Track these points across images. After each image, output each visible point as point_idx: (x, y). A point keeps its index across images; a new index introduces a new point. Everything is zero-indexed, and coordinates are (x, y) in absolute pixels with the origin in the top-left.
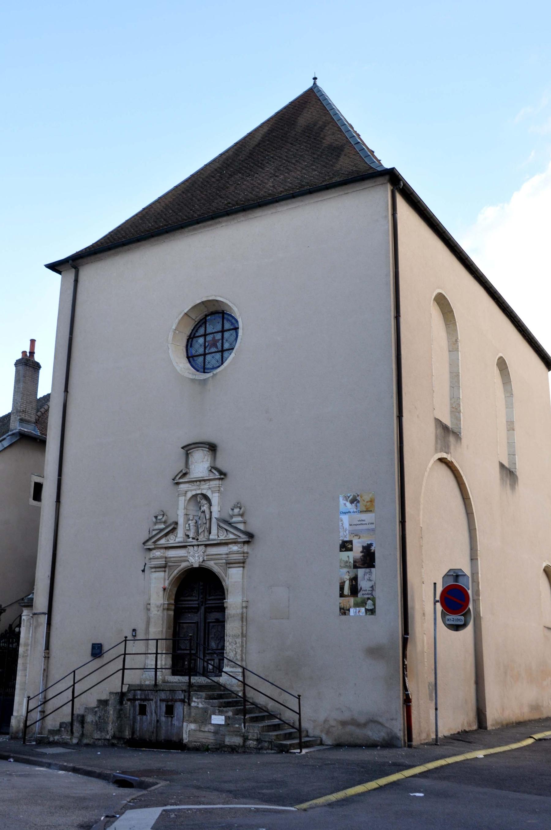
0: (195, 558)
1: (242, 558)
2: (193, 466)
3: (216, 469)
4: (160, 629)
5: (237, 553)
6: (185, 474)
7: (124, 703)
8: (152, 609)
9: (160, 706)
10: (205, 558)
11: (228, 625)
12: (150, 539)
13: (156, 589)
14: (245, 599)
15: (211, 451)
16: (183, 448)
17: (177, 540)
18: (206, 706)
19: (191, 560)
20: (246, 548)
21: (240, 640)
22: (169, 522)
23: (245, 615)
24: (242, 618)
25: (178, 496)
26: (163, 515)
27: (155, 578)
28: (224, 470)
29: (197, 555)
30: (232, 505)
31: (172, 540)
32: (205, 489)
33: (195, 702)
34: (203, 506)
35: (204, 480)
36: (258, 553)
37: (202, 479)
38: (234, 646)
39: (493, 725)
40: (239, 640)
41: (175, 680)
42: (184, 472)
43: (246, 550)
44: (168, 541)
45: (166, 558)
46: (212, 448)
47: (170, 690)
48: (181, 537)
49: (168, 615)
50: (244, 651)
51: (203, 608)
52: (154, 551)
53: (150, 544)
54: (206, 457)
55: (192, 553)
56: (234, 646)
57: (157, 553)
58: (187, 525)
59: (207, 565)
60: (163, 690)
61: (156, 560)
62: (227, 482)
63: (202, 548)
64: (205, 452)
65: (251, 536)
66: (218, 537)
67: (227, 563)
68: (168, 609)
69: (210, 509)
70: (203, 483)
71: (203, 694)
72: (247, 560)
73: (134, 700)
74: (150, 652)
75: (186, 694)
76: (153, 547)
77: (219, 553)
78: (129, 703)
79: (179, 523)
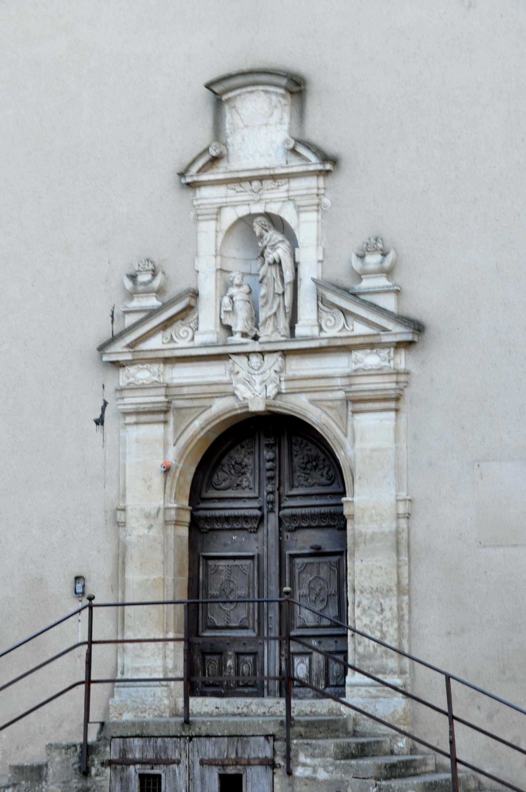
0: (254, 389)
1: (393, 386)
2: (239, 137)
3: (309, 146)
4: (158, 575)
5: (379, 372)
6: (215, 160)
7: (93, 771)
8: (132, 523)
9: (202, 779)
10: (283, 386)
11: (358, 563)
12: (114, 339)
13: (148, 468)
14: (403, 495)
15: (288, 96)
16: (208, 86)
17: (199, 339)
18: (338, 775)
19: (243, 391)
20: (401, 360)
21: (394, 603)
22: (172, 292)
23: (404, 535)
24: (398, 543)
25: (197, 219)
26: (154, 274)
27: (137, 441)
28: (331, 147)
29: (258, 379)
30: (358, 242)
31: (182, 340)
32: (273, 200)
33: (304, 765)
34: (274, 247)
35: (274, 177)
36: (434, 371)
37: (267, 172)
38: (378, 618)
39: (130, 742)
40: (390, 603)
41: (205, 709)
42: (213, 152)
43: (402, 366)
44: (172, 340)
45: (167, 387)
46: (296, 87)
47: (230, 736)
48: (212, 332)
49: (178, 537)
50: (406, 631)
51: (272, 520)
52: (132, 370)
53: (113, 353)
54: (277, 113)
55: (243, 374)
56: (378, 618)
57: (142, 374)
58: (226, 300)
59: (289, 406)
60: (208, 736)
61: (138, 393)
62: (340, 181)
63: (273, 362)
64: (274, 98)
65: (418, 328)
66: (321, 329)
67: (348, 401)
68: (177, 523)
69: (293, 256)
70: (268, 184)
71: (330, 744)
72: (407, 391)
73: (124, 762)
74: (130, 635)
75: (280, 745)
76: (129, 357)
77: (322, 372)
78: (108, 771)
79: (202, 292)
